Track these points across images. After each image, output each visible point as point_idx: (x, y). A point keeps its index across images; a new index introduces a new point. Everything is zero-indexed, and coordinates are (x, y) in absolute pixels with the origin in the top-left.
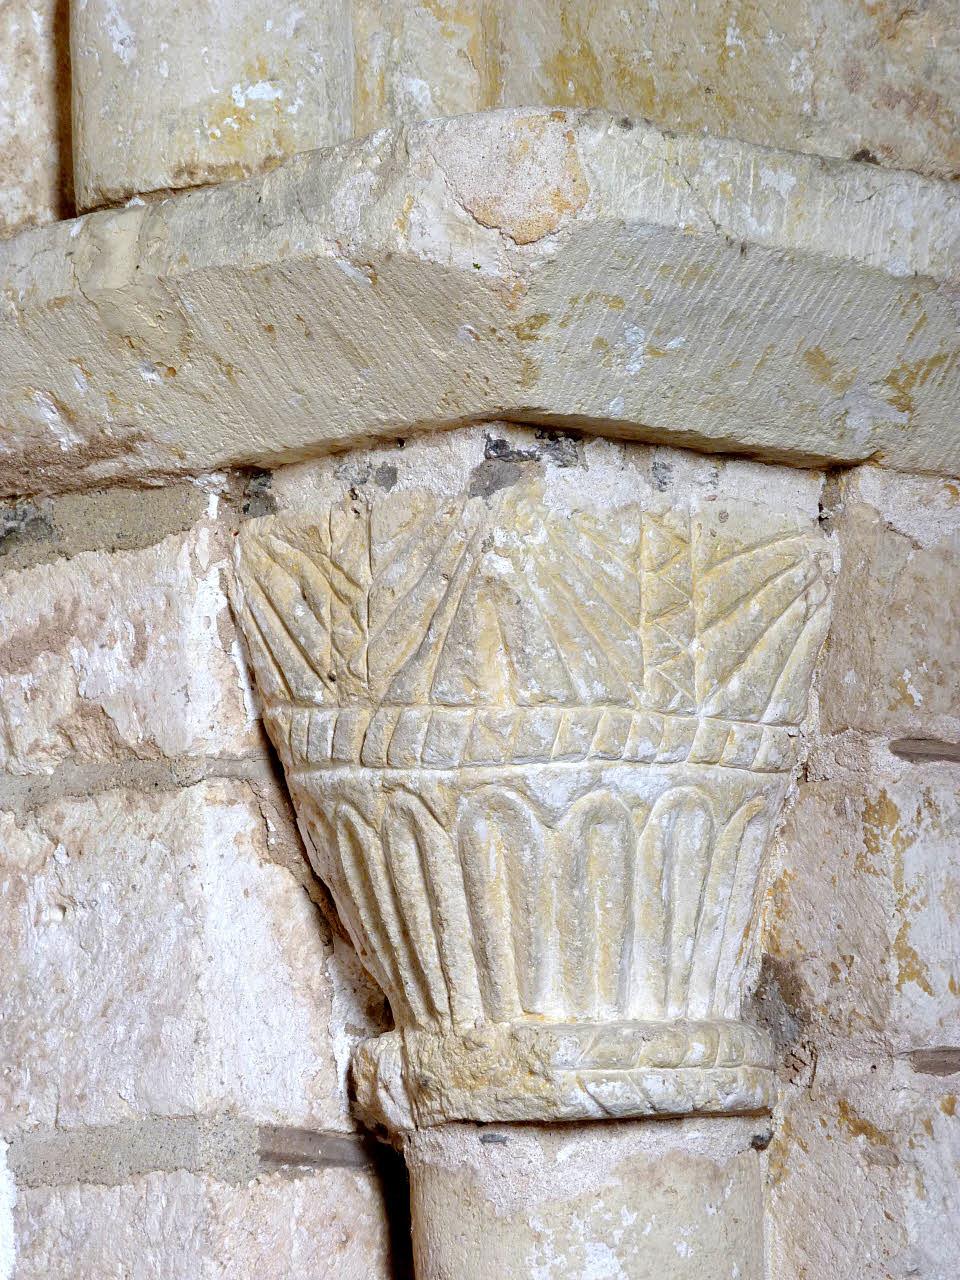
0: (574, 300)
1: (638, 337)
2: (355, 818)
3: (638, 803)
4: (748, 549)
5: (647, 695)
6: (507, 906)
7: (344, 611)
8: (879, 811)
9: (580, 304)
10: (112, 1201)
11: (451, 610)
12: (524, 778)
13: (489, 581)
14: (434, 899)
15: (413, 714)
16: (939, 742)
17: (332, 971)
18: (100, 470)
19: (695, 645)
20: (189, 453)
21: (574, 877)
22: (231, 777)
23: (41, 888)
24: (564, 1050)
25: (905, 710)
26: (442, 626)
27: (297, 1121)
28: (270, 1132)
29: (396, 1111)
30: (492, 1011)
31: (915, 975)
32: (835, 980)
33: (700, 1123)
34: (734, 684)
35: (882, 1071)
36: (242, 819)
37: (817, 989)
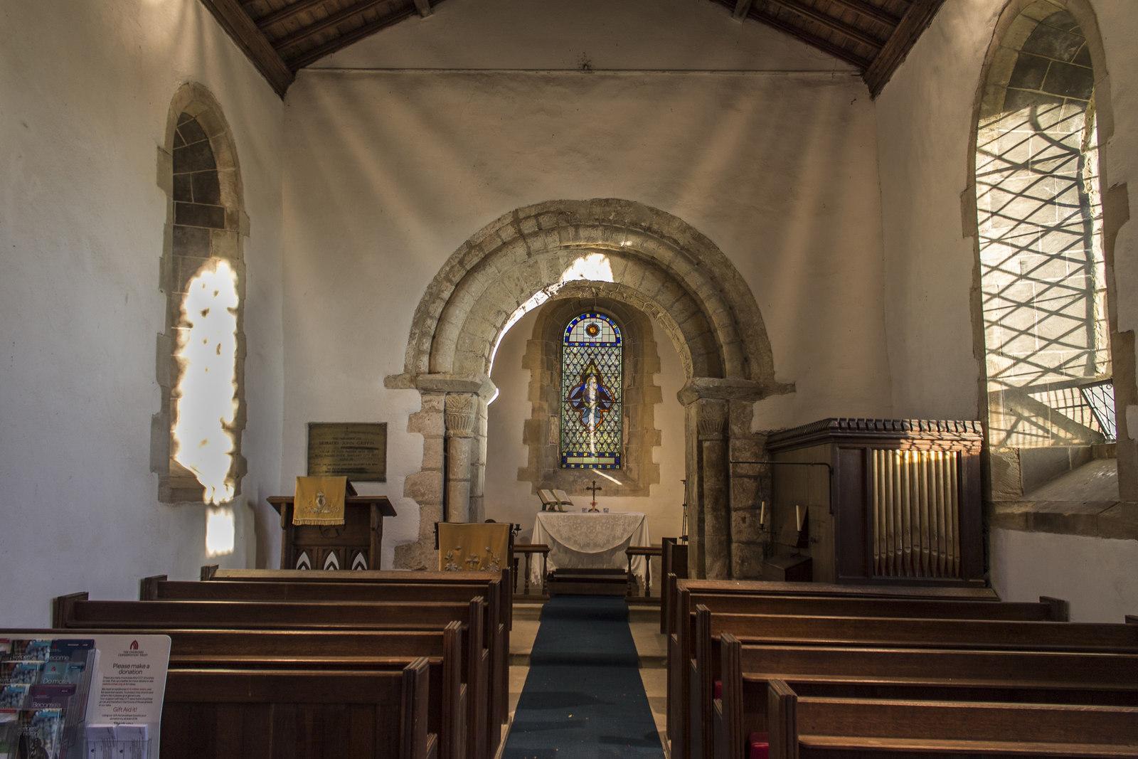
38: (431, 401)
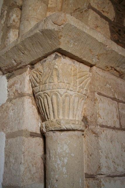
0: (65, 34)
1: (72, 41)
2: (40, 97)
3: (71, 95)
4: (83, 72)
5: (72, 84)
6: (56, 106)
7: (40, 76)
8: (96, 100)
9: (66, 35)
10: (14, 140)
11: (51, 72)
12: (58, 91)
13: (55, 68)
14: (48, 105)
15: (47, 84)
16: (101, 94)
17: (39, 117)
18: (18, 67)
19: (77, 80)
20: (26, 63)
21: (64, 103)
22: (29, 96)
23: (11, 108)
24: (62, 121)
25: (98, 90)
26: (50, 74)
27: (34, 132)
28: (31, 133)
29: (44, 130)
30: (54, 118)
31: (100, 117)
32: (91, 118)
33: (77, 131)
34: (81, 85)
35: (96, 127)
36: (30, 100)
37: (89, 119)
38: (13, 84)
